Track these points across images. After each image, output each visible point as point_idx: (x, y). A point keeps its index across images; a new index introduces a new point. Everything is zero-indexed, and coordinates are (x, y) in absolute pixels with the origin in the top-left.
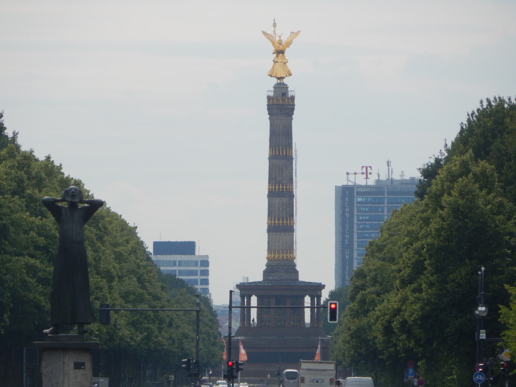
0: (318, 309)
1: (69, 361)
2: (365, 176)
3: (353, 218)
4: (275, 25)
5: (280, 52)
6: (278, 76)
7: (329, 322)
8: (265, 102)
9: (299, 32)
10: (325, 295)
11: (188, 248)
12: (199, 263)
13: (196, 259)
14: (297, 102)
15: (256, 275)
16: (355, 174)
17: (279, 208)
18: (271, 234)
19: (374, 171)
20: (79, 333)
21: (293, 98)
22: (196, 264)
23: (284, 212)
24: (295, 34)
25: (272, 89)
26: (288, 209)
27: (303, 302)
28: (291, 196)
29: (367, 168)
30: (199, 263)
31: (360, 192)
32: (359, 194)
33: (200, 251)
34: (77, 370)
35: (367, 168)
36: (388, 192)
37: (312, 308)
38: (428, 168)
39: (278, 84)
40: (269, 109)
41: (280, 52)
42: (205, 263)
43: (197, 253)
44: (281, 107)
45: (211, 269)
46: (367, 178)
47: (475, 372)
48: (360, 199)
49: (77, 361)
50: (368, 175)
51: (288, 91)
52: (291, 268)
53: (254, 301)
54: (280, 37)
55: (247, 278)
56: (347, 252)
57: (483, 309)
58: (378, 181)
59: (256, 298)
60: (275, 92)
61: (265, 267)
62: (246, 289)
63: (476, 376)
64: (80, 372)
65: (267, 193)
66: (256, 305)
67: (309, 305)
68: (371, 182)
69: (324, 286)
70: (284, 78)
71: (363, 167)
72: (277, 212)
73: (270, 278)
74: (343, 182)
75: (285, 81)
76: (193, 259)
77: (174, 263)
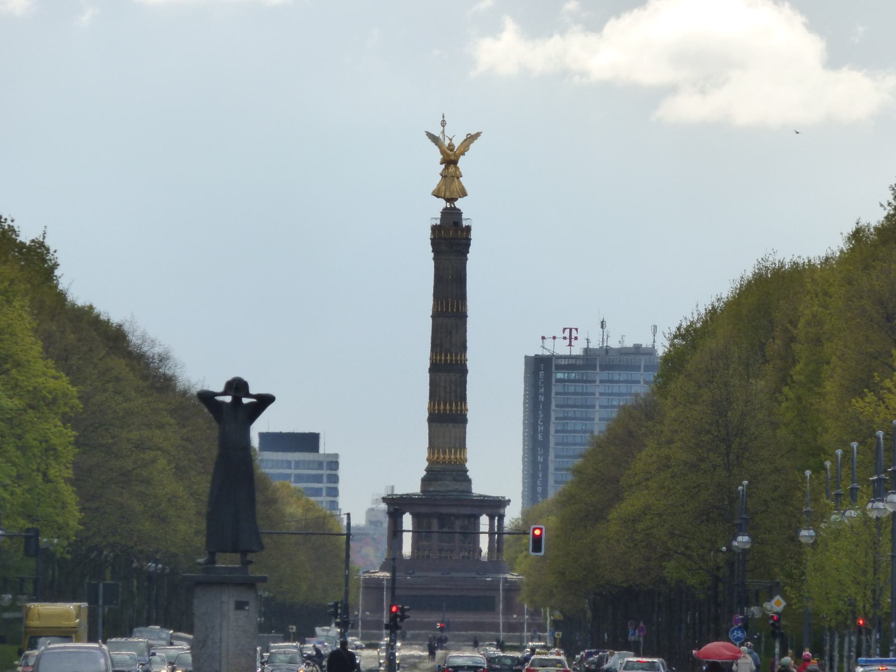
0: (497, 534)
1: (228, 598)
2: (568, 341)
3: (550, 402)
4: (443, 124)
5: (450, 160)
6: (448, 195)
7: (542, 553)
8: (428, 234)
9: (478, 135)
10: (513, 514)
11: (309, 442)
12: (325, 465)
13: (321, 459)
14: (473, 235)
15: (410, 483)
16: (554, 338)
17: (445, 387)
18: (434, 424)
19: (581, 336)
20: (243, 563)
21: (468, 229)
22: (320, 465)
23: (453, 394)
24: (471, 138)
25: (439, 215)
26: (459, 390)
27: (476, 525)
28: (464, 371)
29: (571, 330)
30: (325, 465)
31: (561, 365)
32: (560, 368)
33: (326, 447)
34: (239, 612)
35: (571, 330)
36: (601, 366)
37: (491, 534)
38: (672, 345)
39: (446, 209)
40: (433, 244)
41: (450, 160)
42: (333, 463)
43: (321, 451)
44: (451, 241)
45: (342, 472)
46: (570, 345)
47: (732, 626)
48: (560, 376)
49: (239, 599)
50: (568, 337)
51: (461, 219)
52: (460, 474)
53: (407, 521)
54: (451, 140)
55: (393, 487)
56: (540, 451)
57: (746, 539)
58: (587, 350)
59: (410, 516)
60: (442, 219)
61: (425, 473)
62: (396, 505)
63: (733, 632)
64: (241, 614)
65: (428, 365)
66: (411, 529)
67: (487, 530)
68: (577, 350)
69: (509, 501)
70: (456, 199)
71: (565, 329)
72: (442, 394)
73: (431, 489)
74: (536, 350)
75: (459, 204)
76: (316, 459)
77: (288, 464)
